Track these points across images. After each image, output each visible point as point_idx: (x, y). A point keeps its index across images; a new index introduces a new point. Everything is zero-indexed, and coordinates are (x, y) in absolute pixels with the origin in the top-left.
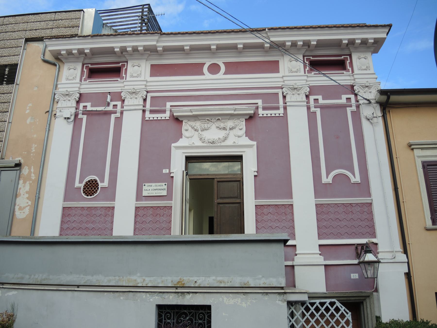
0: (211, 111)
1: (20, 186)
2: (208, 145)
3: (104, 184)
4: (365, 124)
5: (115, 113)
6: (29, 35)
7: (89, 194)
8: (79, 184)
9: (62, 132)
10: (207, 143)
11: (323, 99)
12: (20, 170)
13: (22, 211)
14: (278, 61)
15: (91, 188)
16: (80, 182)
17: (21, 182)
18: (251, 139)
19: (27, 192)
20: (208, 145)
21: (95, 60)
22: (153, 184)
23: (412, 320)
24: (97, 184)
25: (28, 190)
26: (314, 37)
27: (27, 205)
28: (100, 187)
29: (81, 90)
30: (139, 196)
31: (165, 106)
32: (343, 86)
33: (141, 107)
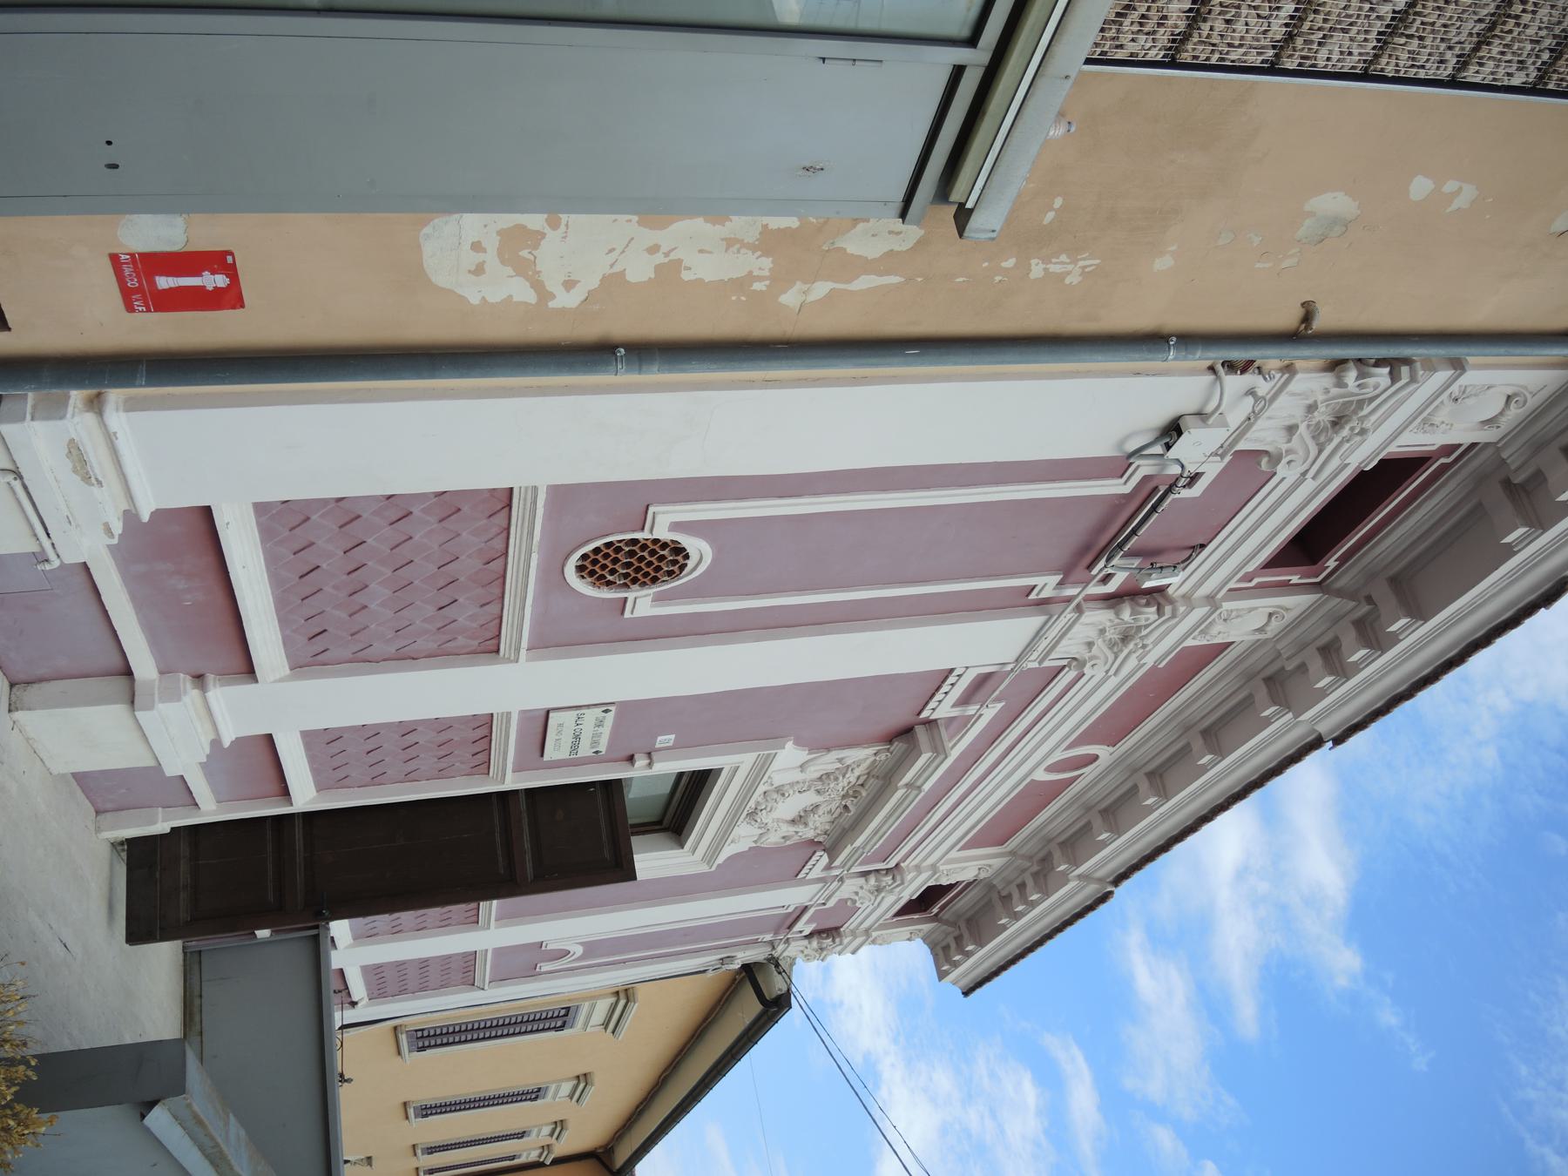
2: (752, 804)
3: (643, 603)
7: (595, 562)
8: (663, 525)
10: (758, 803)
13: (491, 258)
15: (651, 562)
16: (676, 526)
19: (669, 272)
20: (752, 804)
21: (1452, 485)
24: (654, 580)
25: (686, 276)
26: (958, 749)
27: (553, 284)
32: (691, 213)
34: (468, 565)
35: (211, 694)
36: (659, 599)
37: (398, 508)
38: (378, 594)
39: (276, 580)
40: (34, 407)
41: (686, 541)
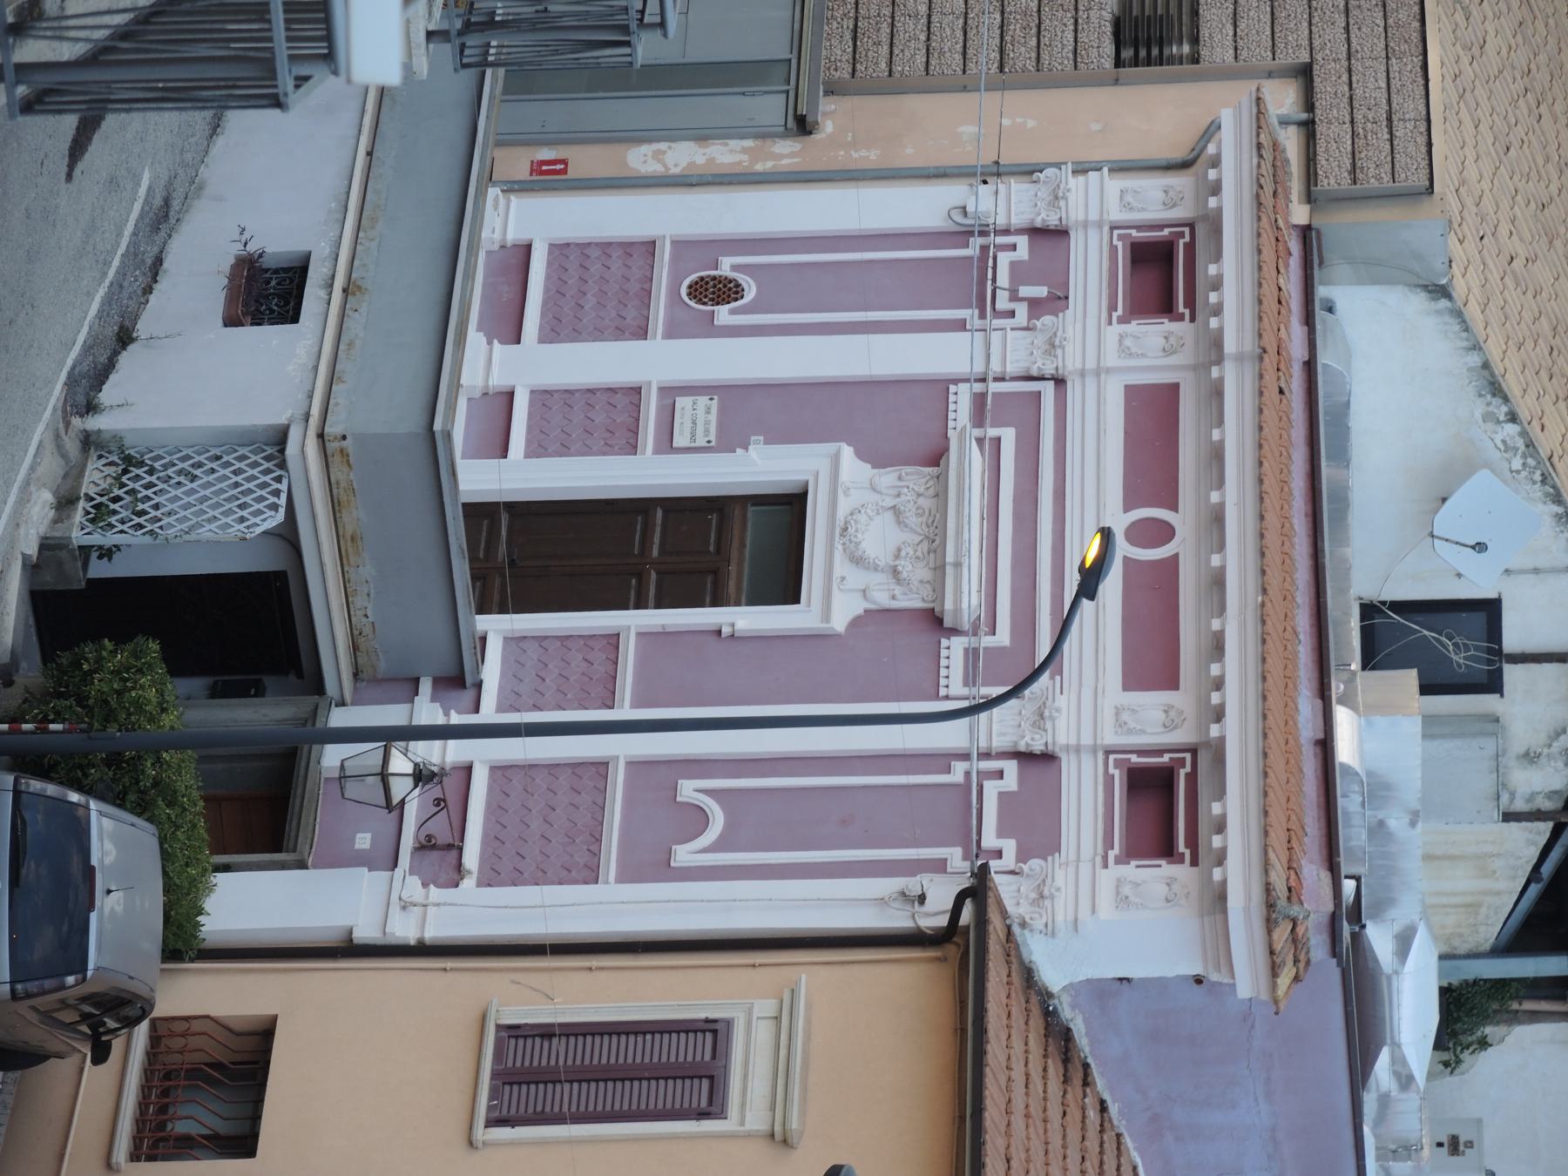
0: (958, 511)
1: (733, 143)
3: (723, 314)
4: (888, 886)
5: (982, 316)
6: (1329, 87)
8: (726, 267)
9: (922, 206)
11: (1001, 794)
12: (787, 134)
13: (649, 159)
14: (1177, 688)
15: (720, 291)
16: (735, 268)
17: (749, 143)
18: (856, 623)
19: (711, 161)
22: (713, 417)
23: (202, 946)
27: (670, 165)
28: (716, 308)
29: (1081, 232)
30: (670, 393)
31: (996, 424)
33: (996, 367)
34: (634, 287)
35: (107, 403)
36: (733, 312)
37: (606, 247)
38: (590, 302)
39: (547, 290)
40: (659, 587)
41: (742, 278)
